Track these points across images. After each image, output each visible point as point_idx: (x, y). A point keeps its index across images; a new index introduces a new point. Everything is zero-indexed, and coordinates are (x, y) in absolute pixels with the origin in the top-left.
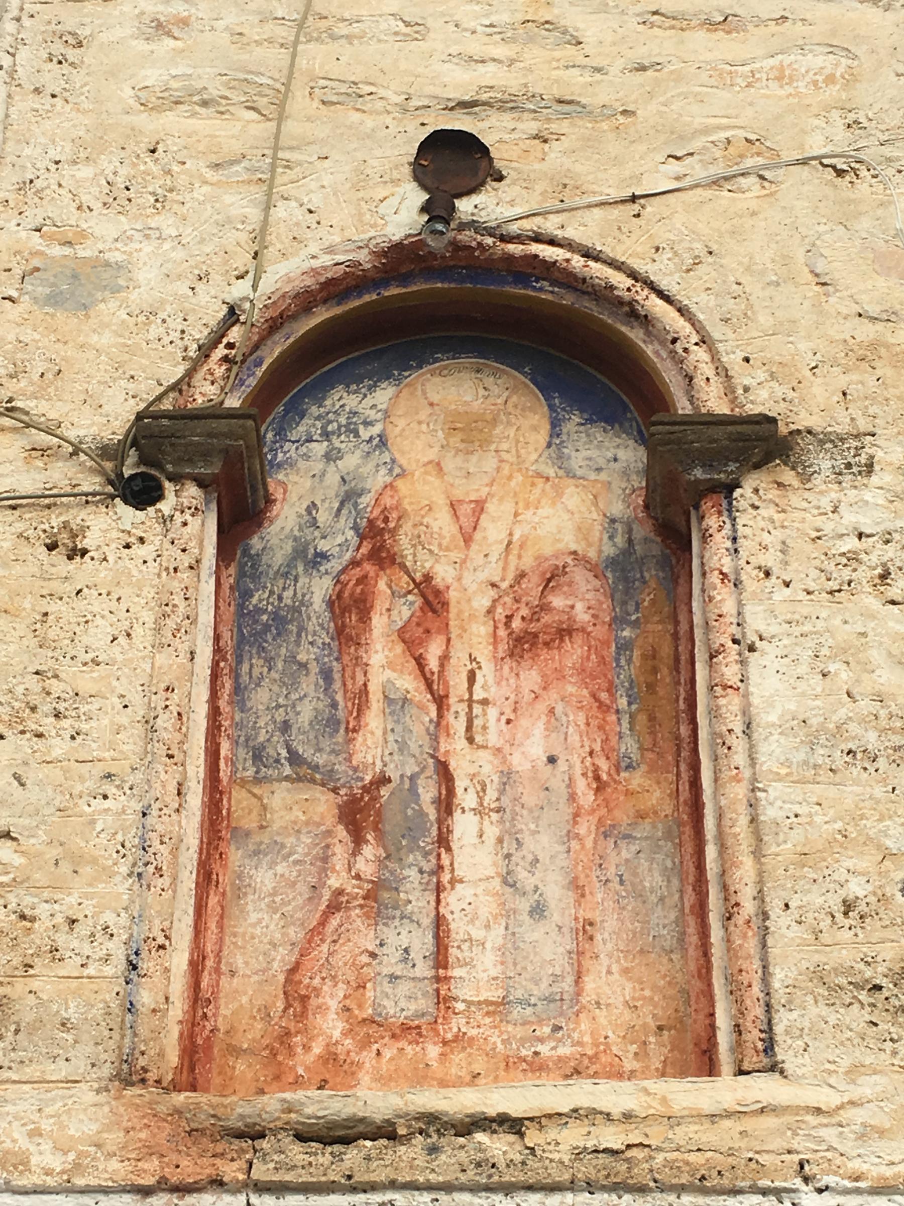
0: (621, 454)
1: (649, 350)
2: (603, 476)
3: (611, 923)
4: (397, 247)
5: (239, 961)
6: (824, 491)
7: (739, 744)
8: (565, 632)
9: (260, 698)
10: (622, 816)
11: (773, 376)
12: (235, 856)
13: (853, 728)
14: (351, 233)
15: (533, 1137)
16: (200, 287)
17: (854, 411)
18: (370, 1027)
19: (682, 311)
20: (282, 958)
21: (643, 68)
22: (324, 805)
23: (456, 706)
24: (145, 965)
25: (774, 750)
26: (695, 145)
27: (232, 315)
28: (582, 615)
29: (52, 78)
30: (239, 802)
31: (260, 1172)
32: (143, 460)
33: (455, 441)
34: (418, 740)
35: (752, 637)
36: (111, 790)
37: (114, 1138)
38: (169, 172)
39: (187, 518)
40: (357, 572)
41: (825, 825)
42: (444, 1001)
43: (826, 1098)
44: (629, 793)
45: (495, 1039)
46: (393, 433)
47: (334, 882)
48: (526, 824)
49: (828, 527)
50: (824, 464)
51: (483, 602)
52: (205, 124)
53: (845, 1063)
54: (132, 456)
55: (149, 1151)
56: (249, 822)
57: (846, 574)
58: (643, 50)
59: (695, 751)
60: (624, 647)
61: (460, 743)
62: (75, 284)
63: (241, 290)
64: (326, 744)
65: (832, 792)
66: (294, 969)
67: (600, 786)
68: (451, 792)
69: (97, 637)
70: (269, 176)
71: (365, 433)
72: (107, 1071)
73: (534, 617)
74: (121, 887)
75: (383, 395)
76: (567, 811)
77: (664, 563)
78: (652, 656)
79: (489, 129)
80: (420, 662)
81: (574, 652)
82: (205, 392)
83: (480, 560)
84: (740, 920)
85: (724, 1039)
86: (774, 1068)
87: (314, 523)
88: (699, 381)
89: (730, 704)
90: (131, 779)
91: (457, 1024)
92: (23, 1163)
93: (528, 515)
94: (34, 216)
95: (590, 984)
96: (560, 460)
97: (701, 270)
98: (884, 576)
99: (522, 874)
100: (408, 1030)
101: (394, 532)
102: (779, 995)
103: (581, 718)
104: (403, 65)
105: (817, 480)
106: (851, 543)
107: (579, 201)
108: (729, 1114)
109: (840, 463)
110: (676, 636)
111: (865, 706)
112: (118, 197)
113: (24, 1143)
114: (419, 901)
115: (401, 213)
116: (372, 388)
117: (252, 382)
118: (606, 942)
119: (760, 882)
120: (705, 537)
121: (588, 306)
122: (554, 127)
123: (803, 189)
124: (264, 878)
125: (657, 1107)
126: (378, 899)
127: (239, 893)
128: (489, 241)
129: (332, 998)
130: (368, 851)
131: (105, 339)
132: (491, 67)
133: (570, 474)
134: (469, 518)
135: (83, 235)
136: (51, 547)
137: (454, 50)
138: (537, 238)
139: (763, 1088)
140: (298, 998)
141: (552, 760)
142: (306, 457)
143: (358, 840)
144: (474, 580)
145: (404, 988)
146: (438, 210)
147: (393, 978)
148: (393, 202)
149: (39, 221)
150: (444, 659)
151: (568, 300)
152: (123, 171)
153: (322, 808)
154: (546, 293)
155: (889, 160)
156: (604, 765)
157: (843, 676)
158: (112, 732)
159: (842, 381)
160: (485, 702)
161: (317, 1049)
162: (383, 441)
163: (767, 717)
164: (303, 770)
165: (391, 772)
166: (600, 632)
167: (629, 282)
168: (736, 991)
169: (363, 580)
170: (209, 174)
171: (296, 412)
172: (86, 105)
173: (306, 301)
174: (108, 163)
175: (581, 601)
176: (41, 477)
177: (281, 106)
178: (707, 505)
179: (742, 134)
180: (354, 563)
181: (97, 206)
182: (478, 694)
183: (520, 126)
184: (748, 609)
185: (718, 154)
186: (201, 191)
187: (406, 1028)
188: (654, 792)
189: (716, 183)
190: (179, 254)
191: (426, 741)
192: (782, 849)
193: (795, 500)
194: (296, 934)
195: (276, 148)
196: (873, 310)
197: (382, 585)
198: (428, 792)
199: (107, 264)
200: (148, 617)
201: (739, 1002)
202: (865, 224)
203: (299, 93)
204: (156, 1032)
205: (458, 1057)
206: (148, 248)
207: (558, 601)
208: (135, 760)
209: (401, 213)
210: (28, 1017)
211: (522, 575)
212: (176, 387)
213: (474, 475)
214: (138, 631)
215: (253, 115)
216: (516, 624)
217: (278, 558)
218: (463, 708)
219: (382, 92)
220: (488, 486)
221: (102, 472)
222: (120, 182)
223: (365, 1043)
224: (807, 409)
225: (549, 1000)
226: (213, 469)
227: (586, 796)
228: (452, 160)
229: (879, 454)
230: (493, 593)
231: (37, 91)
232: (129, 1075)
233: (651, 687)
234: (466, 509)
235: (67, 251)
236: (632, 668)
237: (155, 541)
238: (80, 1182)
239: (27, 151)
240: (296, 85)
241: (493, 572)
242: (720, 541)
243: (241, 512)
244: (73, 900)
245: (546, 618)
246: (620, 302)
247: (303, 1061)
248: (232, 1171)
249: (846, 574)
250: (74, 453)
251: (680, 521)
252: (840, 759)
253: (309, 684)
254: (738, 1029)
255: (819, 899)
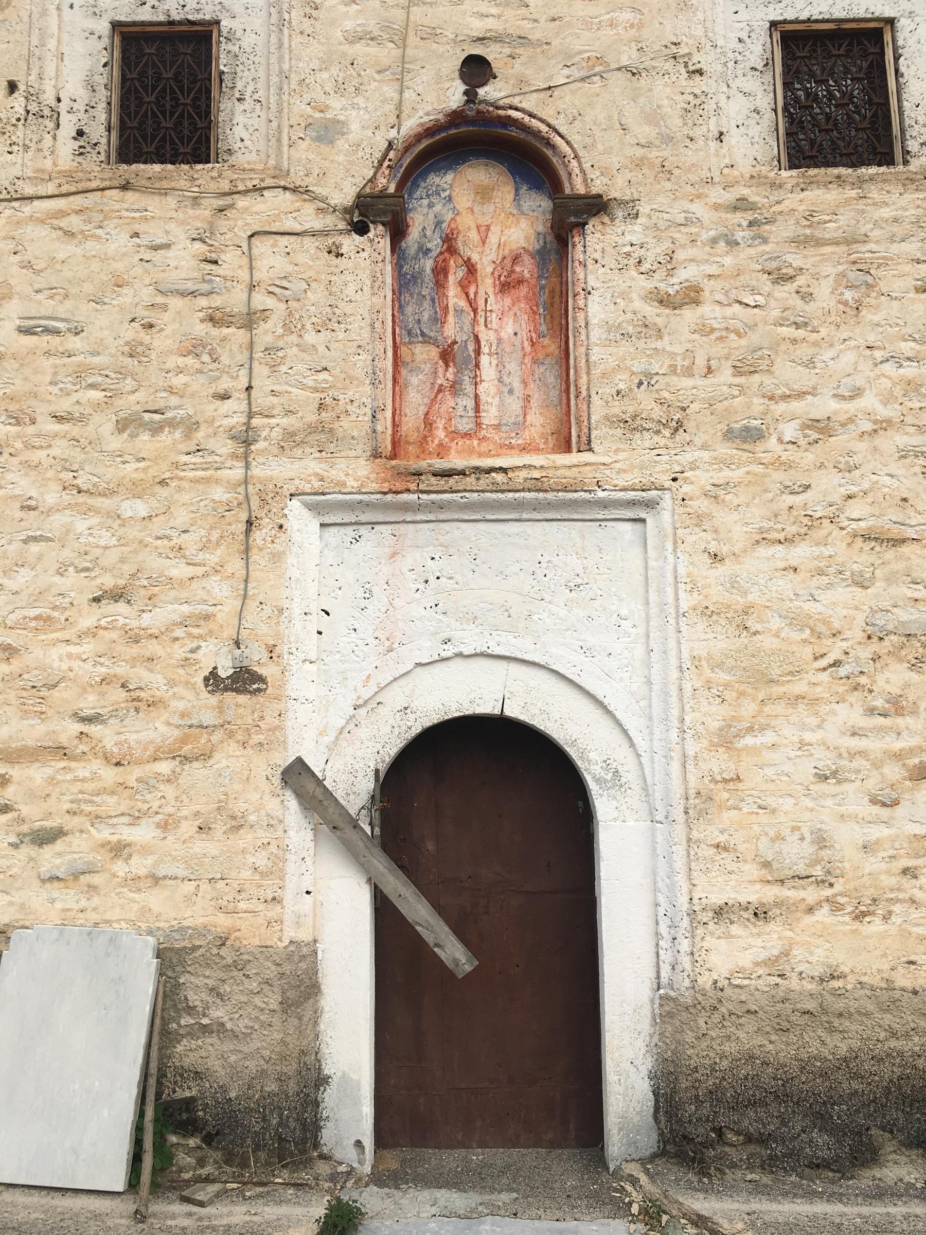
0: (543, 204)
1: (554, 160)
2: (535, 214)
3: (536, 396)
4: (454, 112)
5: (408, 411)
6: (619, 226)
7: (583, 331)
8: (520, 282)
9: (409, 310)
10: (540, 356)
11: (602, 174)
12: (404, 372)
13: (624, 325)
14: (436, 105)
15: (510, 474)
16: (377, 132)
17: (633, 190)
18: (454, 434)
19: (568, 143)
20: (422, 410)
21: (554, 20)
22: (434, 352)
23: (481, 313)
24: (378, 416)
25: (596, 334)
26: (576, 60)
27: (390, 145)
28: (527, 275)
29: (307, 25)
30: (404, 351)
31: (421, 487)
32: (361, 214)
33: (478, 198)
34: (467, 327)
35: (590, 289)
36: (361, 352)
37: (373, 476)
38: (359, 75)
39: (379, 236)
40: (442, 257)
41: (612, 363)
42: (479, 425)
43: (607, 460)
44: (543, 347)
45: (497, 438)
46: (454, 194)
47: (439, 382)
48: (506, 359)
49: (620, 242)
50: (620, 214)
51: (490, 269)
52: (373, 50)
53: (614, 448)
54: (357, 212)
55: (385, 480)
56: (408, 359)
57: (626, 261)
58: (554, 10)
59: (567, 330)
60: (543, 288)
61: (482, 327)
62: (327, 132)
63: (393, 133)
64: (434, 328)
65: (615, 350)
66: (427, 414)
67: (533, 344)
68: (479, 347)
69: (350, 290)
70: (401, 75)
71: (443, 195)
72: (369, 454)
73: (509, 276)
74: (368, 389)
75: (449, 177)
76: (521, 354)
77: (558, 252)
78: (552, 292)
79: (491, 53)
80: (467, 295)
81: (524, 290)
82: (382, 181)
83: (488, 251)
84: (581, 398)
85: (574, 439)
86: (590, 450)
87: (425, 236)
88: (574, 176)
89: (581, 316)
90: (368, 348)
91: (483, 433)
92: (344, 484)
93: (506, 232)
94: (307, 97)
95: (529, 418)
96: (519, 207)
97: (576, 122)
98: (640, 262)
99: (505, 378)
100: (467, 435)
101: (456, 239)
102: (593, 425)
103: (526, 317)
104: (454, 19)
105: (617, 221)
106: (628, 249)
107: (527, 89)
108: (575, 466)
109: (626, 214)
110: (561, 283)
111: (629, 316)
112: (340, 88)
113: (343, 478)
114: (469, 388)
115: (454, 96)
116: (445, 174)
117: (399, 175)
118: (534, 402)
119: (589, 384)
120: (574, 246)
121: (530, 139)
122: (517, 51)
123: (618, 81)
124: (414, 380)
125: (552, 464)
126: (455, 388)
127: (406, 386)
128: (491, 109)
129: (440, 423)
130: (451, 370)
131: (341, 158)
132: (491, 19)
133: (523, 213)
134: (484, 231)
135: (327, 107)
136: (329, 252)
137: (475, 10)
138: (511, 108)
139: (587, 457)
140: (429, 424)
141: (516, 334)
142: (421, 206)
143: (447, 366)
144: (486, 260)
145: (465, 420)
146: (471, 96)
147: (461, 416)
148: (452, 89)
149: (308, 100)
150: (476, 293)
151: (522, 136)
152: (341, 75)
153: (434, 354)
154: (514, 133)
155: (654, 68)
156: (534, 336)
157: (622, 303)
158: (359, 329)
159: (629, 176)
160: (491, 311)
161: (436, 442)
162: (450, 199)
163: (593, 321)
164: (427, 339)
165: (458, 339)
166: (533, 282)
167: (547, 129)
168: (579, 423)
169: (444, 260)
170: (377, 77)
171: (415, 185)
172: (323, 41)
173: (419, 138)
174: (334, 71)
175: (526, 269)
176: (322, 222)
177: (404, 40)
178: (575, 232)
179: (594, 54)
180: (441, 253)
181: (332, 92)
182: (489, 308)
183: (504, 50)
184: (589, 277)
185: (584, 64)
186: (374, 85)
187: (466, 434)
188: (551, 346)
189: (583, 79)
190: (367, 117)
191: (470, 327)
192: (596, 372)
193: (608, 230)
194: (427, 401)
195: (403, 63)
196: (643, 142)
197: (452, 262)
198: (471, 347)
199: (338, 122)
200: (368, 283)
201: (580, 427)
202: (642, 100)
203: (411, 33)
204: (384, 439)
205: (484, 444)
206: (354, 113)
207: (518, 269)
208: (368, 340)
209: (454, 96)
210: (341, 435)
211: (504, 258)
212: (370, 181)
213: (487, 213)
214: (365, 288)
215: (392, 45)
216: (502, 278)
217: (412, 251)
218: (483, 313)
219: (446, 33)
220: (491, 218)
221: (345, 220)
222: (340, 80)
223: (452, 440)
224: (616, 189)
225: (515, 424)
226: (388, 218)
227: (528, 349)
228: (476, 69)
229: (641, 209)
230: (494, 266)
231: (301, 33)
232: (376, 455)
233: (552, 304)
234: (483, 229)
235: (322, 115)
236: (545, 297)
237: (368, 250)
238: (363, 490)
239: (301, 65)
240: (410, 29)
241: (493, 256)
242: (579, 248)
243: (398, 232)
244: (351, 393)
245: (513, 276)
246: (543, 138)
247: (432, 446)
248: (413, 487)
249: (626, 261)
250: (334, 211)
251: (564, 234)
252: (619, 337)
253: (426, 304)
254: (579, 436)
255: (609, 390)
